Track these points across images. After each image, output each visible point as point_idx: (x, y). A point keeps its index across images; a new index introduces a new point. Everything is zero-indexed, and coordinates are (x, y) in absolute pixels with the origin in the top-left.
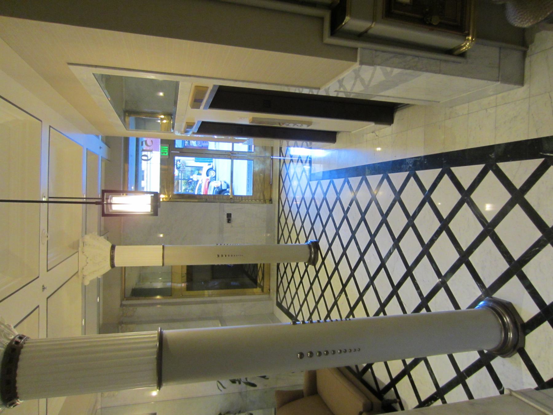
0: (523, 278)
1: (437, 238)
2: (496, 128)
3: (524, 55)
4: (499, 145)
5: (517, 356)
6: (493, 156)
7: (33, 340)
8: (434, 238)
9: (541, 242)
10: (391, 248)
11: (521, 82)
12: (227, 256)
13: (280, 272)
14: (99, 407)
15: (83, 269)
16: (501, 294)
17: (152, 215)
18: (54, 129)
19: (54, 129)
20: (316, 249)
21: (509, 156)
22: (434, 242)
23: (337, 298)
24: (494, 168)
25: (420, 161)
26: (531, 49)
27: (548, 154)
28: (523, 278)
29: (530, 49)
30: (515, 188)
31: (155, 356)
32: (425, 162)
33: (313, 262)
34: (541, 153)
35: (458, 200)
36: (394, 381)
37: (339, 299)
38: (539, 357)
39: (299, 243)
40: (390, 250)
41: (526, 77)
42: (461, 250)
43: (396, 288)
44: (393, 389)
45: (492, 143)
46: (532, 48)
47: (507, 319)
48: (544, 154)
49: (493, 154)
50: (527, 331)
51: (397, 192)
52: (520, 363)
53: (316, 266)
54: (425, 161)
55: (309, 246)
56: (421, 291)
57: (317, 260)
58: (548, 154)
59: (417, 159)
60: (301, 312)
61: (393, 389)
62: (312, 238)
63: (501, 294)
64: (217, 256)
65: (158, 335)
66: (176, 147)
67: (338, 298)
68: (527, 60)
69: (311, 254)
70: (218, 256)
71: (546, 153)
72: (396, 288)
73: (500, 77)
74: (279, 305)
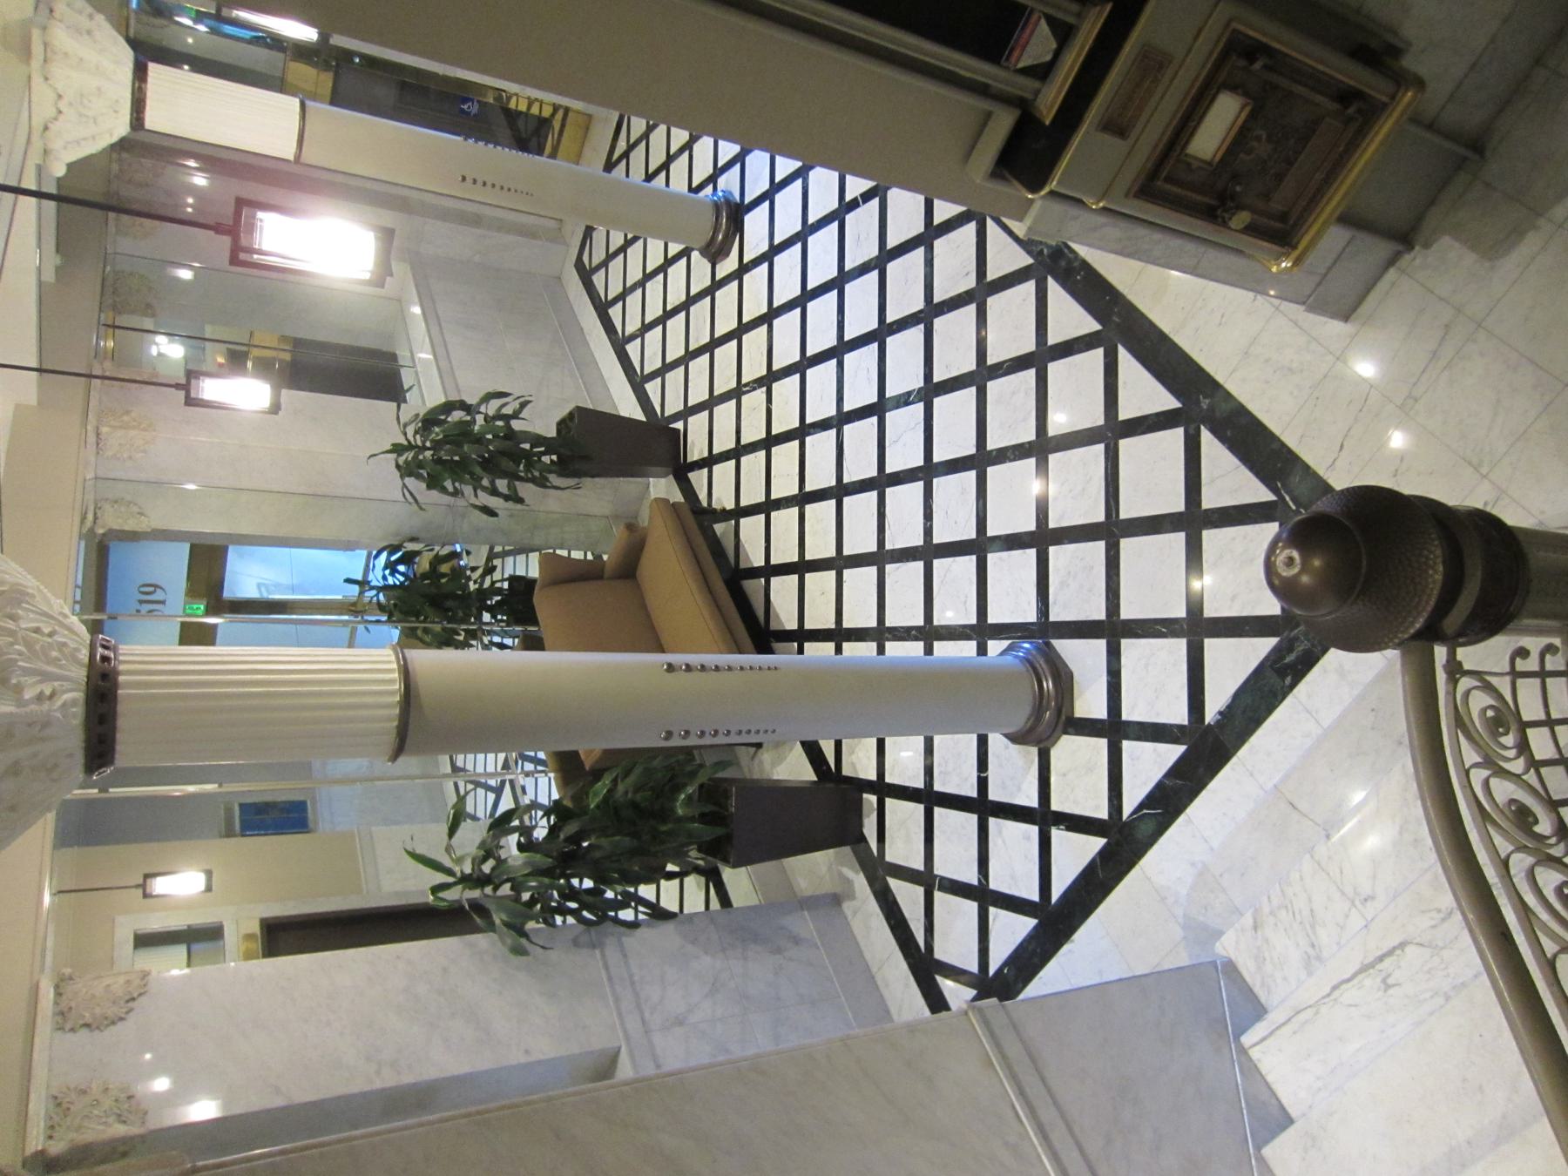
0: (1114, 654)
1: (1014, 460)
2: (1246, 353)
3: (1391, 262)
4: (1228, 395)
5: (1034, 751)
6: (1205, 403)
8: (1009, 454)
9: (1176, 627)
10: (914, 390)
11: (1346, 318)
14: (90, 475)
15: (46, 128)
16: (1067, 648)
17: (368, 283)
20: (732, 229)
21: (1229, 433)
22: (1004, 462)
23: (747, 385)
24: (1191, 431)
25: (1070, 262)
26: (1414, 259)
27: (1287, 498)
28: (1114, 654)
29: (1412, 254)
30: (1199, 503)
31: (395, 723)
32: (1078, 277)
33: (715, 253)
34: (1279, 485)
35: (1094, 425)
37: (748, 392)
38: (1064, 775)
40: (909, 394)
41: (1365, 308)
42: (1044, 521)
43: (887, 255)
45: (1220, 378)
46: (1415, 259)
47: (1048, 685)
48: (1283, 492)
49: (1207, 401)
50: (1070, 730)
51: (984, 282)
52: (1032, 762)
53: (718, 267)
54: (1079, 274)
55: (717, 207)
56: (931, 526)
57: (727, 254)
58: (1287, 498)
59: (1066, 251)
63: (1067, 648)
64: (460, 179)
65: (399, 673)
67: (747, 389)
68: (1392, 274)
70: (464, 179)
71: (1287, 493)
72: (887, 255)
73: (1312, 298)
74: (586, 275)
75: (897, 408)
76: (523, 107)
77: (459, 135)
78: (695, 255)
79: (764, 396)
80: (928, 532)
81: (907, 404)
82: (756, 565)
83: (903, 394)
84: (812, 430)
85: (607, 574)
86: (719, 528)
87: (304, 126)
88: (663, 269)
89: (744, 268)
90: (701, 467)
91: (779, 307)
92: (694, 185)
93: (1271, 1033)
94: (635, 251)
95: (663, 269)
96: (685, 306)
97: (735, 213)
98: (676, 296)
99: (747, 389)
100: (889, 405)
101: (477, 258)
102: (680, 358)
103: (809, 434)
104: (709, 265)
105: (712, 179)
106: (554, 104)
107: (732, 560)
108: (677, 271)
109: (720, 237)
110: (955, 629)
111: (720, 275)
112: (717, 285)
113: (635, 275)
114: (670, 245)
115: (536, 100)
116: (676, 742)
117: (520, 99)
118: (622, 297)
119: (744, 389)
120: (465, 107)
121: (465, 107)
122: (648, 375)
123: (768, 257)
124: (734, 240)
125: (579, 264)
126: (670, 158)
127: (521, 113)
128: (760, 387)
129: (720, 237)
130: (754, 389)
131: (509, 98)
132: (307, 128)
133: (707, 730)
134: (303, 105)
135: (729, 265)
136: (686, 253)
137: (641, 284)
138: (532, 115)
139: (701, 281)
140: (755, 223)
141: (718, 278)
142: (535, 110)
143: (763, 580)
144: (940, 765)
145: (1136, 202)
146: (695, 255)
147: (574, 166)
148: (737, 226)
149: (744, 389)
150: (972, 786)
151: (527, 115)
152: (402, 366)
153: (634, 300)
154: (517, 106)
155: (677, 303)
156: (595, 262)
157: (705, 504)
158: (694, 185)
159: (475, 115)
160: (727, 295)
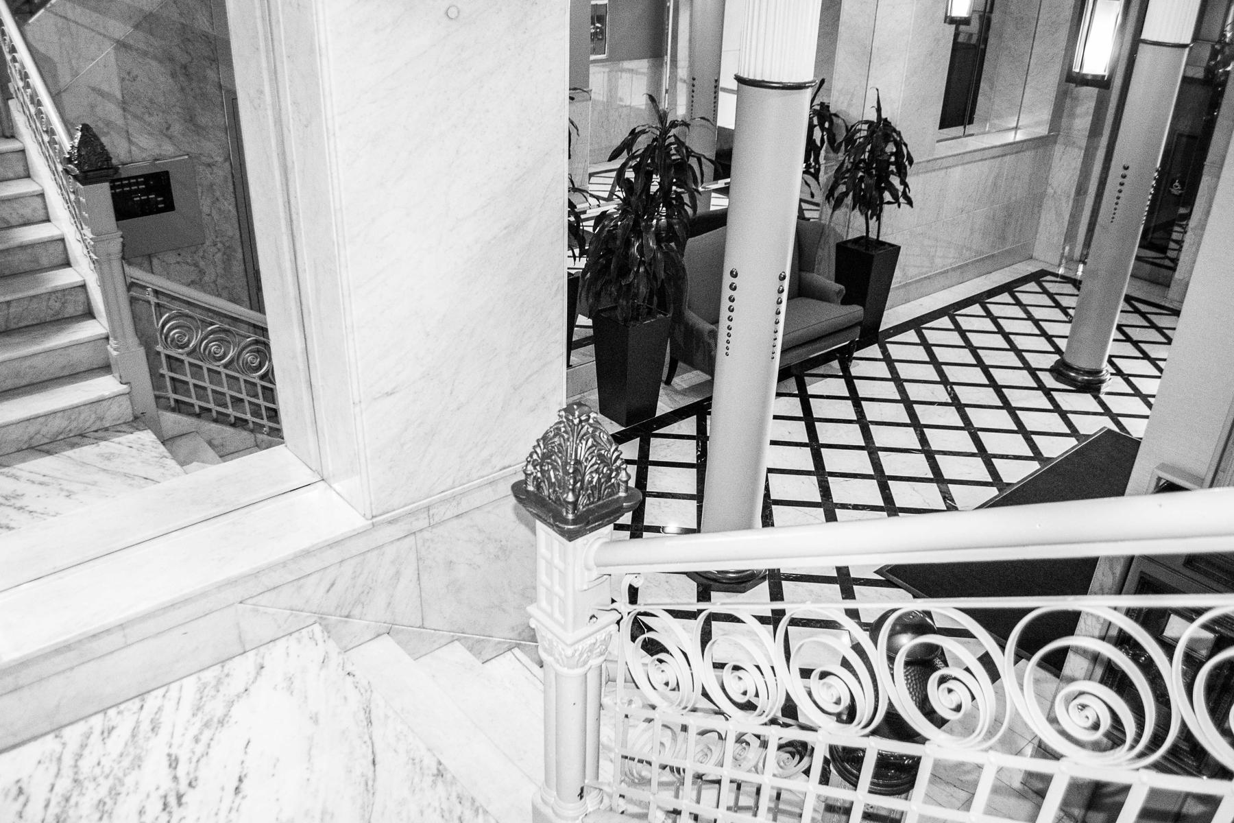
7: (1056, 458)
12: (1121, 180)
13: (1060, 282)
18: (940, 404)
19: (940, 404)
23: (952, 389)
33: (1060, 371)
36: (850, 381)
37: (947, 390)
39: (1153, 396)
44: (841, 374)
57: (1057, 379)
60: (1149, 316)
61: (841, 374)
62: (1112, 384)
66: (636, 466)
67: (949, 389)
69: (1077, 371)
70: (1126, 168)
74: (1037, 277)
75: (941, 492)
76: (1175, 236)
77: (1160, 166)
78: (1057, 357)
79: (944, 401)
80: (844, 506)
81: (944, 498)
82: (808, 388)
83: (951, 496)
84: (918, 432)
85: (803, 274)
86: (835, 364)
87: (1169, 46)
88: (1027, 366)
89: (1048, 393)
90: (883, 353)
91: (1016, 415)
92: (1113, 359)
93: (524, 665)
94: (1057, 314)
95: (1027, 366)
96: (993, 383)
97: (1091, 386)
98: (979, 418)
99: (949, 389)
100: (943, 487)
101: (1050, 191)
102: (971, 343)
103: (915, 430)
104: (1049, 367)
105: (1119, 372)
106: (1178, 260)
107: (809, 372)
108: (1042, 344)
109: (1073, 374)
110: (770, 519)
111: (1040, 374)
112: (1033, 372)
113: (1037, 313)
114: (1066, 340)
115: (1181, 247)
116: (727, 280)
117: (1176, 252)
118: (1018, 303)
119: (948, 387)
120: (1177, 184)
121: (1177, 184)
122: (932, 350)
123: (1057, 408)
124: (1067, 384)
125: (1043, 273)
126: (1136, 344)
127: (1171, 235)
128: (951, 398)
129: (1073, 374)
130: (949, 394)
131: (1181, 226)
132: (1165, 48)
133: (191, 792)
134: (1184, 46)
135: (1049, 381)
136: (1058, 350)
137: (993, 383)
138: (1168, 244)
139: (1034, 361)
140: (1085, 401)
141: (1038, 372)
142: (1172, 245)
143: (797, 392)
144: (666, 503)
145: (1136, 579)
146: (1057, 357)
147: (1129, 274)
148: (1083, 388)
149: (948, 387)
150: (652, 522)
151: (1169, 239)
152: (965, 127)
153: (1017, 312)
154: (1176, 231)
155: (1016, 343)
156: (1047, 285)
157: (856, 354)
158: (1113, 359)
159: (1170, 191)
160: (1024, 378)
